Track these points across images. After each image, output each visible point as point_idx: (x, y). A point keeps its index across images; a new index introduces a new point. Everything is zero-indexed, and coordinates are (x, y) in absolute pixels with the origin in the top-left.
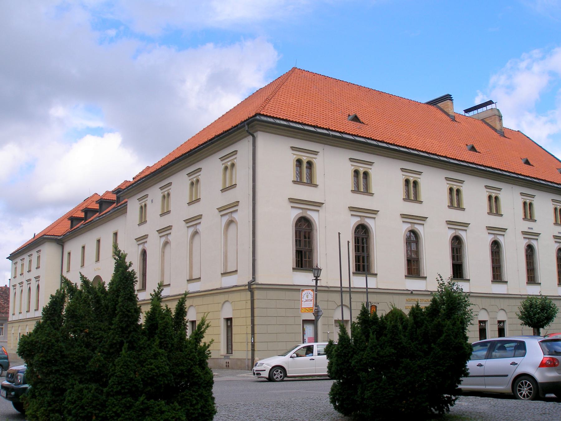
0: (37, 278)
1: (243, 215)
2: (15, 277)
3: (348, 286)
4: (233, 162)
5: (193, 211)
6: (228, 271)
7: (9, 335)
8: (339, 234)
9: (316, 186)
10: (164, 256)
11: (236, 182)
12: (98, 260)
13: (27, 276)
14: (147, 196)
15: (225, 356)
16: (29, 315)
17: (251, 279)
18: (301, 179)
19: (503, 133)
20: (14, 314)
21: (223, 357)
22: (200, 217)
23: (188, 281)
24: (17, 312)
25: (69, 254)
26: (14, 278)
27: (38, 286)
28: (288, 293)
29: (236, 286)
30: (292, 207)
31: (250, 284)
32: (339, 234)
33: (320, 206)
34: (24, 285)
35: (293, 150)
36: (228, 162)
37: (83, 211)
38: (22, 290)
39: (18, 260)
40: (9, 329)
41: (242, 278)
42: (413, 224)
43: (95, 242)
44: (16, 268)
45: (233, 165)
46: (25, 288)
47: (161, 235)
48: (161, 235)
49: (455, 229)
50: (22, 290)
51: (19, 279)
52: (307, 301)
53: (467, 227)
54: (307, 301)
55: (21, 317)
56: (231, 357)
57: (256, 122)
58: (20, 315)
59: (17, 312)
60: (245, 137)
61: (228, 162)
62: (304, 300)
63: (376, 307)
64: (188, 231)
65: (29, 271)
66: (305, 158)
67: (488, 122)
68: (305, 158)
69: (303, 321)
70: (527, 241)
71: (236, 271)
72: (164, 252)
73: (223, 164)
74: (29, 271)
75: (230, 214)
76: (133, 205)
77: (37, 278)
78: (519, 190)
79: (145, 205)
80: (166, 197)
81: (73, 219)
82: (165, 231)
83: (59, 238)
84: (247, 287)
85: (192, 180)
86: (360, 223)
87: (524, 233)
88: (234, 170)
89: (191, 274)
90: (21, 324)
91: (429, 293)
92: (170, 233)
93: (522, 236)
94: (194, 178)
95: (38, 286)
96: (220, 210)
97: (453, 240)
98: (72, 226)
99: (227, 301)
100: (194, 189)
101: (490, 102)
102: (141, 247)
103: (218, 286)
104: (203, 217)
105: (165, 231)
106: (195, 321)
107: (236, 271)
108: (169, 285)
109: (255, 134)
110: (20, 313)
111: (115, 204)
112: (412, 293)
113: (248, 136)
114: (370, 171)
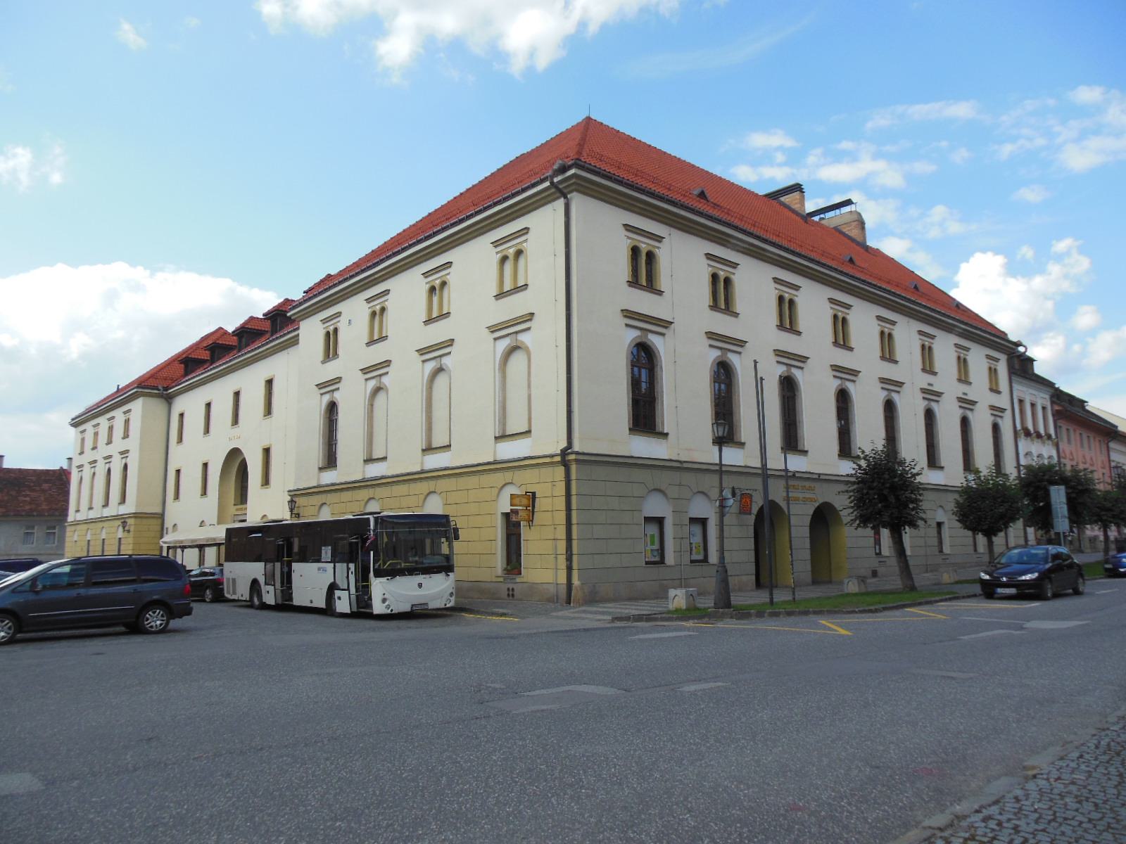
2: (82, 453)
3: (718, 462)
4: (519, 247)
5: (438, 332)
8: (756, 362)
9: (660, 293)
10: (372, 411)
12: (235, 421)
13: (104, 450)
14: (339, 314)
16: (107, 512)
18: (637, 280)
19: (867, 249)
20: (78, 511)
21: (501, 579)
23: (496, 438)
25: (182, 415)
26: (80, 454)
27: (126, 467)
29: (446, 469)
30: (627, 325)
31: (564, 453)
32: (756, 362)
33: (666, 327)
34: (84, 469)
35: (627, 230)
36: (436, 279)
37: (206, 348)
38: (94, 474)
39: (88, 426)
40: (68, 534)
42: (789, 367)
43: (263, 384)
44: (83, 440)
45: (383, 310)
46: (101, 469)
47: (123, 456)
48: (123, 456)
49: (841, 378)
50: (94, 474)
51: (90, 455)
53: (856, 376)
55: (92, 515)
56: (518, 580)
58: (91, 511)
61: (436, 279)
64: (321, 398)
65: (94, 448)
66: (645, 245)
67: (844, 230)
68: (644, 246)
70: (926, 402)
71: (529, 432)
72: (372, 405)
73: (497, 253)
75: (514, 335)
76: (311, 331)
77: (124, 453)
78: (918, 326)
79: (336, 330)
80: (378, 315)
82: (376, 370)
84: (558, 459)
85: (374, 309)
86: (720, 360)
87: (924, 391)
88: (385, 315)
90: (92, 526)
91: (816, 476)
92: (387, 373)
93: (921, 395)
94: (436, 280)
97: (838, 394)
99: (373, 498)
100: (435, 299)
101: (848, 202)
102: (326, 398)
104: (455, 344)
105: (376, 370)
107: (529, 432)
108: (384, 459)
110: (91, 508)
112: (794, 475)
113: (558, 198)
114: (732, 277)
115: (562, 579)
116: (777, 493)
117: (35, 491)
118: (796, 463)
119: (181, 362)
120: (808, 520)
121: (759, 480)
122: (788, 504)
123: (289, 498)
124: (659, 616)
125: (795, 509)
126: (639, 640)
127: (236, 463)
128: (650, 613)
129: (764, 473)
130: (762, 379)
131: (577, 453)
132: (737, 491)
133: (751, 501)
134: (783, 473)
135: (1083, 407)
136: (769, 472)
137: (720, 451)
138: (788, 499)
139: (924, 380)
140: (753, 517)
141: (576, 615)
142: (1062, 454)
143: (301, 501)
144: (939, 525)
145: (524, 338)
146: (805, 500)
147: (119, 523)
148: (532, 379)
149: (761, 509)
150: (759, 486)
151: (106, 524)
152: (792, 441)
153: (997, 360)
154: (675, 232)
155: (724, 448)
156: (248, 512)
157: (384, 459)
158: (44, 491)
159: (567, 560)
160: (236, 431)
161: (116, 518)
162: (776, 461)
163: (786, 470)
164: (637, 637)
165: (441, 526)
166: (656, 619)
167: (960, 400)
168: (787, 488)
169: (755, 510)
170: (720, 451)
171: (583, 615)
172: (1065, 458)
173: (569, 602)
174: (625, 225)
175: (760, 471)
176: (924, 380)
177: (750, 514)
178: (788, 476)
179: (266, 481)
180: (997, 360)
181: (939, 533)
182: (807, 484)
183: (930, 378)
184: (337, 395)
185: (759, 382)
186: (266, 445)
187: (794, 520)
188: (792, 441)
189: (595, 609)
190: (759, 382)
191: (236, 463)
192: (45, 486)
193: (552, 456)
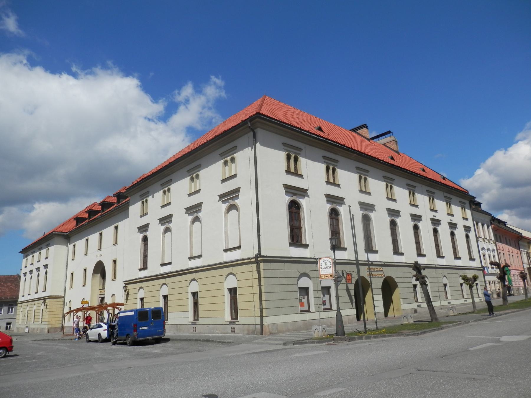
0: (46, 266)
1: (245, 200)
6: (194, 255)
7: (18, 313)
11: (236, 171)
15: (230, 322)
17: (257, 252)
21: (228, 323)
22: (200, 205)
24: (26, 294)
28: (286, 266)
37: (86, 212)
41: (252, 253)
52: (325, 268)
54: (325, 268)
55: (29, 298)
56: (237, 323)
57: (257, 119)
59: (26, 294)
60: (246, 133)
62: (322, 267)
63: (351, 274)
69: (300, 288)
74: (26, 267)
81: (78, 219)
83: (66, 234)
89: (191, 252)
95: (46, 273)
96: (221, 197)
98: (77, 224)
103: (186, 268)
105: (166, 220)
106: (167, 296)
108: (201, 256)
109: (255, 131)
111: (116, 205)
113: (249, 132)
115: (258, 321)
116: (364, 272)
117: (4, 286)
118: (372, 257)
119: (74, 219)
120: (380, 286)
121: (355, 266)
122: (370, 278)
123: (124, 285)
124: (307, 341)
125: (374, 280)
126: (297, 357)
127: (100, 269)
128: (303, 339)
129: (357, 263)
130: (353, 215)
131: (264, 257)
132: (344, 272)
133: (352, 277)
134: (367, 263)
135: (505, 225)
136: (360, 262)
137: (334, 252)
138: (371, 275)
139: (431, 215)
140: (353, 285)
141: (266, 341)
142: (498, 248)
143: (129, 286)
144: (445, 285)
145: (237, 202)
146: (378, 276)
147: (42, 301)
148: (241, 220)
149: (357, 281)
150: (356, 270)
151: (36, 302)
152: (369, 249)
153: (465, 203)
154: (307, 146)
155: (336, 251)
156: (105, 293)
157: (201, 256)
158: (8, 286)
159: (260, 311)
160: (100, 252)
161: (41, 299)
162: (363, 256)
163: (368, 261)
164: (295, 355)
165: (158, 316)
166: (306, 343)
167: (432, 220)
168: (369, 269)
169: (354, 281)
170: (334, 252)
171: (269, 342)
172: (500, 250)
173: (262, 334)
174: (283, 144)
175: (355, 262)
176: (431, 215)
177: (352, 283)
178: (370, 264)
179: (114, 278)
180: (465, 203)
181: (445, 289)
182: (379, 268)
183: (435, 214)
184: (148, 234)
185: (352, 217)
186: (114, 258)
187: (374, 286)
188: (369, 249)
189: (275, 338)
190: (352, 217)
191: (100, 269)
192: (9, 284)
193: (252, 258)
